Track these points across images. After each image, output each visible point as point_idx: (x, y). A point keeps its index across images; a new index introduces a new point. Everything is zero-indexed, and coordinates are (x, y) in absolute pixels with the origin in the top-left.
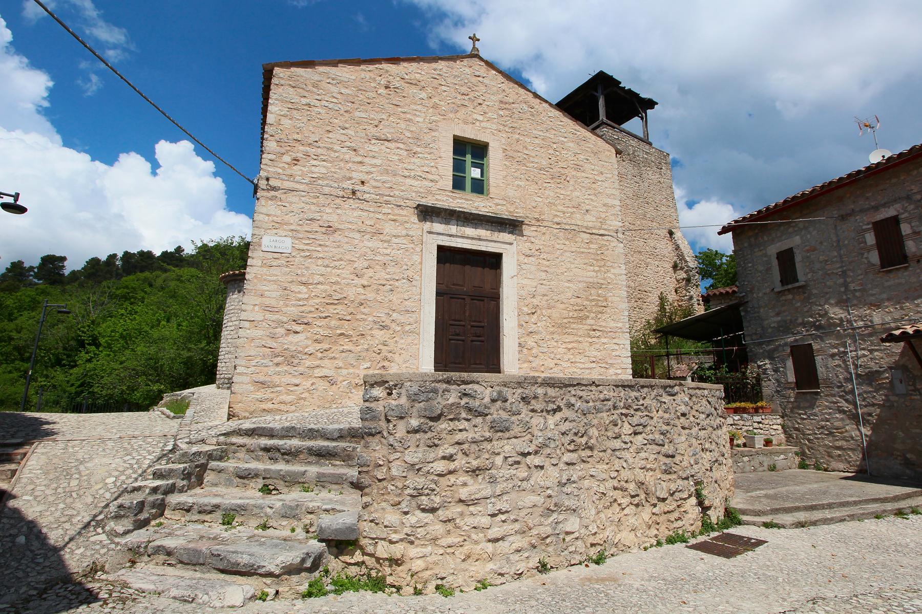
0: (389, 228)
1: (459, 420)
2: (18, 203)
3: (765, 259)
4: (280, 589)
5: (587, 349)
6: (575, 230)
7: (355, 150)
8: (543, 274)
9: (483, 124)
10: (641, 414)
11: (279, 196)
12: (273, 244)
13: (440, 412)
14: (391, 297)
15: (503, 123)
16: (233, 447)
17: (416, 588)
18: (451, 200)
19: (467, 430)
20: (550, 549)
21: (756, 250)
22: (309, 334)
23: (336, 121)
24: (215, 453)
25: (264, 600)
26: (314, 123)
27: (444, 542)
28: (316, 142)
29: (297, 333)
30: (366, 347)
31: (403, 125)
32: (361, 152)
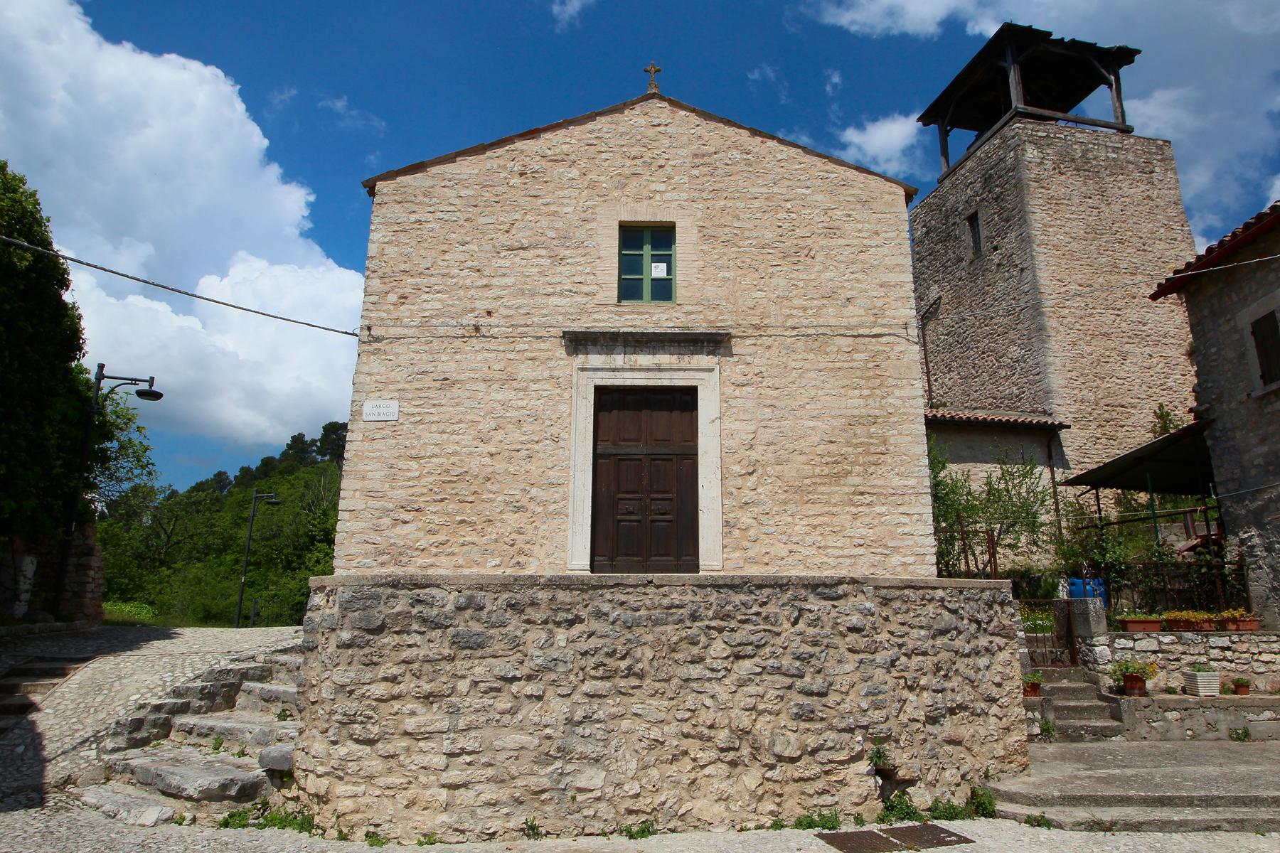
0: (525, 371)
1: (408, 633)
2: (153, 388)
3: (1236, 337)
4: (198, 815)
5: (848, 525)
6: (824, 334)
7: (478, 271)
9: (668, 196)
10: (754, 628)
11: (382, 348)
12: (376, 411)
13: (380, 623)
14: (528, 467)
15: (698, 187)
16: (277, 666)
17: (341, 832)
18: (617, 318)
19: (419, 646)
20: (548, 808)
21: (1221, 321)
22: (420, 524)
24: (252, 671)
25: (180, 824)
26: (425, 245)
27: (381, 781)
28: (428, 269)
29: (405, 522)
30: (494, 536)
31: (544, 222)
32: (487, 272)
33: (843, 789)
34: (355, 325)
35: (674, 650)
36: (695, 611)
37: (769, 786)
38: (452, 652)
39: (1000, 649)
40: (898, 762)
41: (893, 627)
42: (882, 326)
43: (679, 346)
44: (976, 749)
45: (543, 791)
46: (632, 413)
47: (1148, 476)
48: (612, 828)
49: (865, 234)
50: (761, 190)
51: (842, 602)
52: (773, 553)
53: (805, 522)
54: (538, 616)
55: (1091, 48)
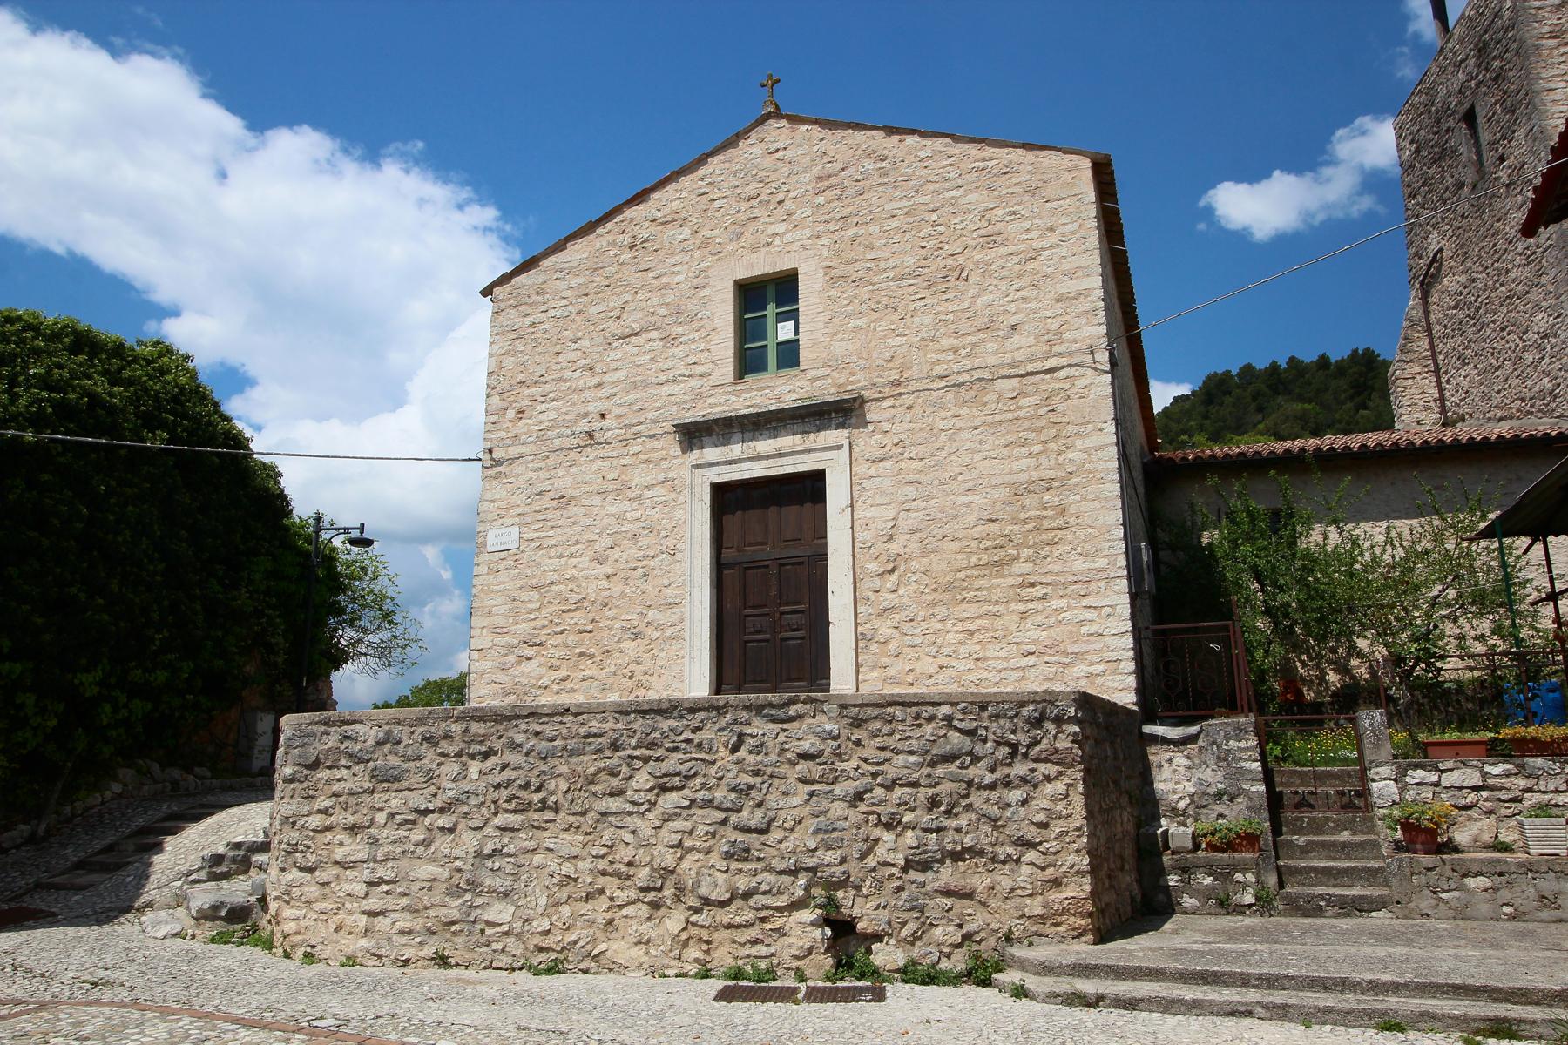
0: (639, 477)
5: (1013, 627)
6: (980, 380)
7: (591, 369)
8: (912, 488)
9: (788, 237)
10: (682, 756)
12: (498, 540)
14: (644, 587)
18: (734, 398)
20: (459, 940)
23: (566, 333)
26: (539, 349)
27: (318, 906)
29: (529, 659)
30: (612, 669)
31: (655, 300)
33: (781, 939)
34: (477, 449)
35: (592, 782)
36: (617, 740)
37: (693, 931)
38: (371, 785)
39: (1048, 779)
40: (856, 912)
41: (869, 752)
42: (1058, 355)
43: (803, 422)
44: (993, 904)
45: (453, 923)
46: (757, 512)
48: (520, 964)
49: (1034, 234)
50: (899, 204)
51: (795, 724)
52: (919, 670)
53: (959, 627)
54: (452, 749)
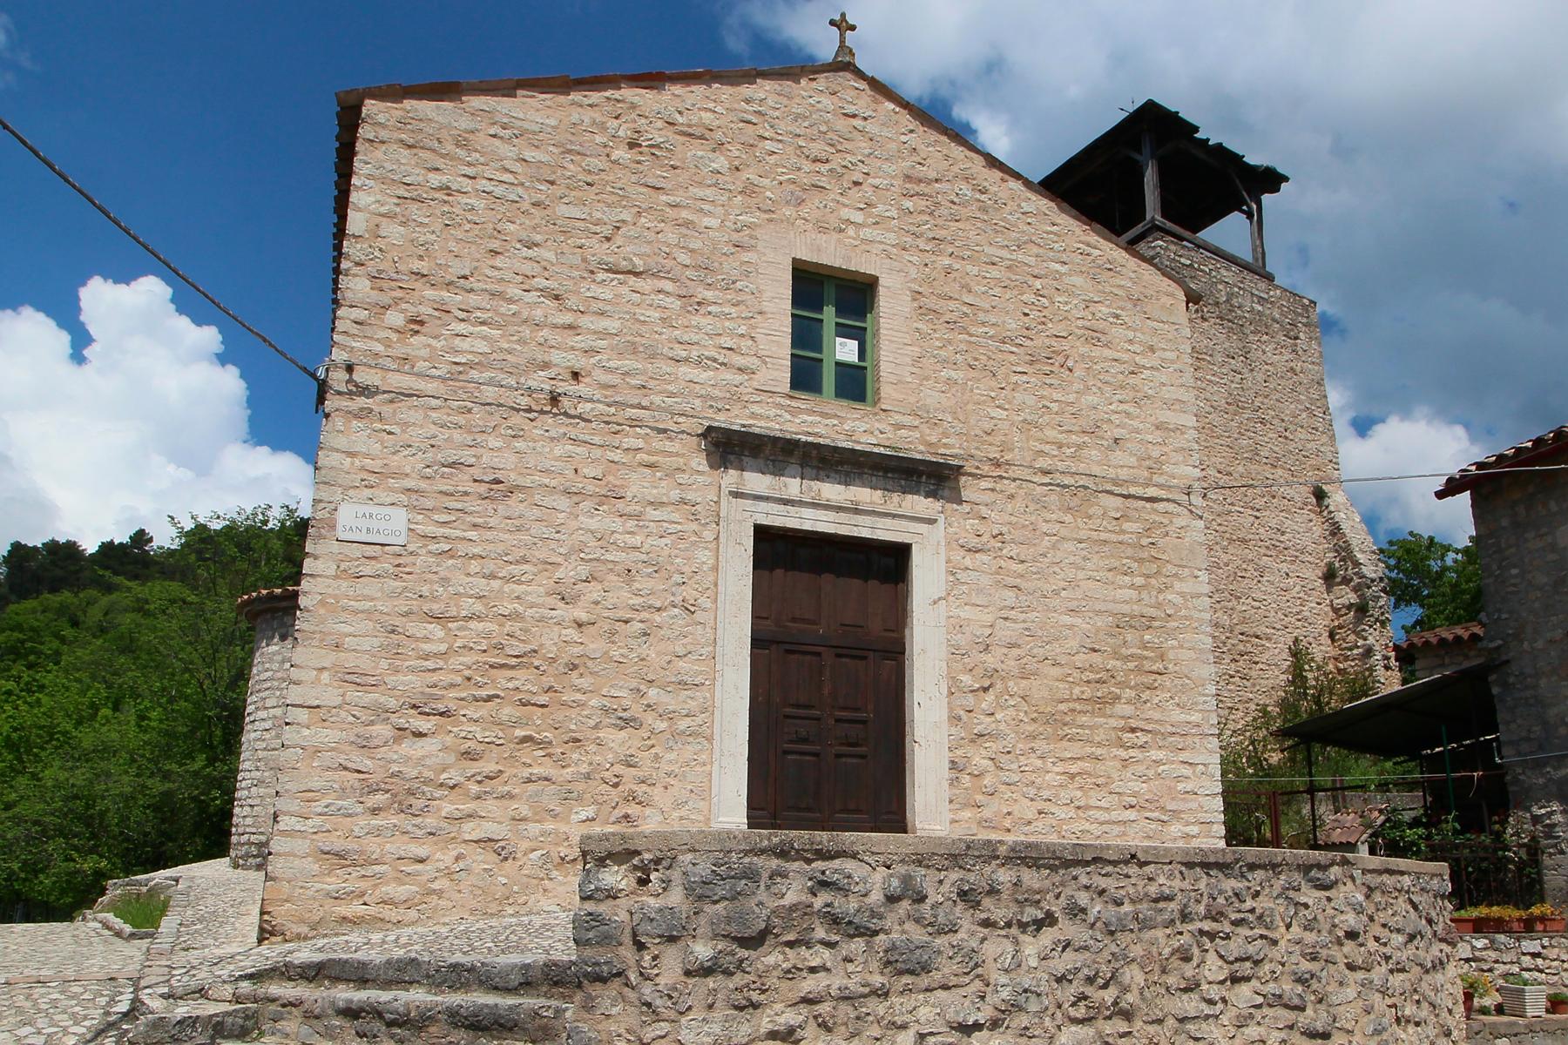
0: (639, 485)
5: (1115, 775)
7: (557, 298)
9: (867, 233)
12: (364, 524)
16: (273, 1007)
19: (828, 970)
22: (449, 739)
26: (459, 234)
28: (465, 277)
29: (420, 735)
30: (584, 768)
31: (671, 236)
43: (885, 477)
47: (1444, 729)
53: (1059, 768)
55: (1236, 159)
